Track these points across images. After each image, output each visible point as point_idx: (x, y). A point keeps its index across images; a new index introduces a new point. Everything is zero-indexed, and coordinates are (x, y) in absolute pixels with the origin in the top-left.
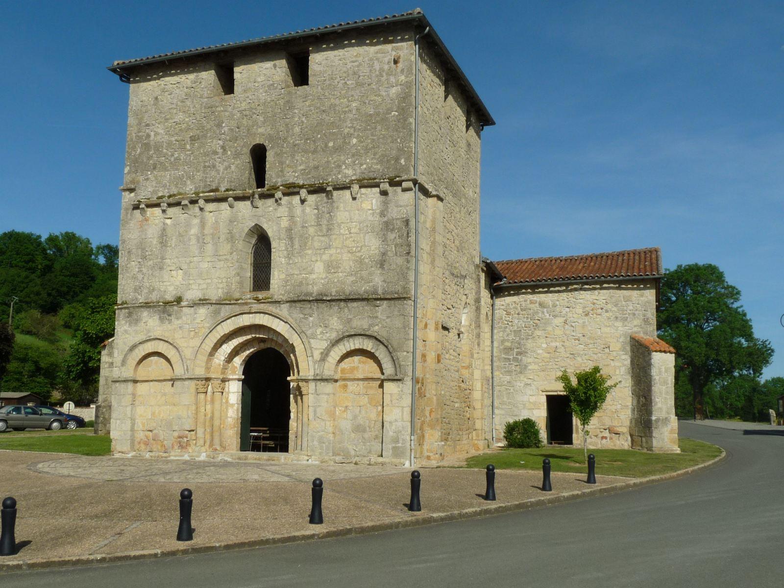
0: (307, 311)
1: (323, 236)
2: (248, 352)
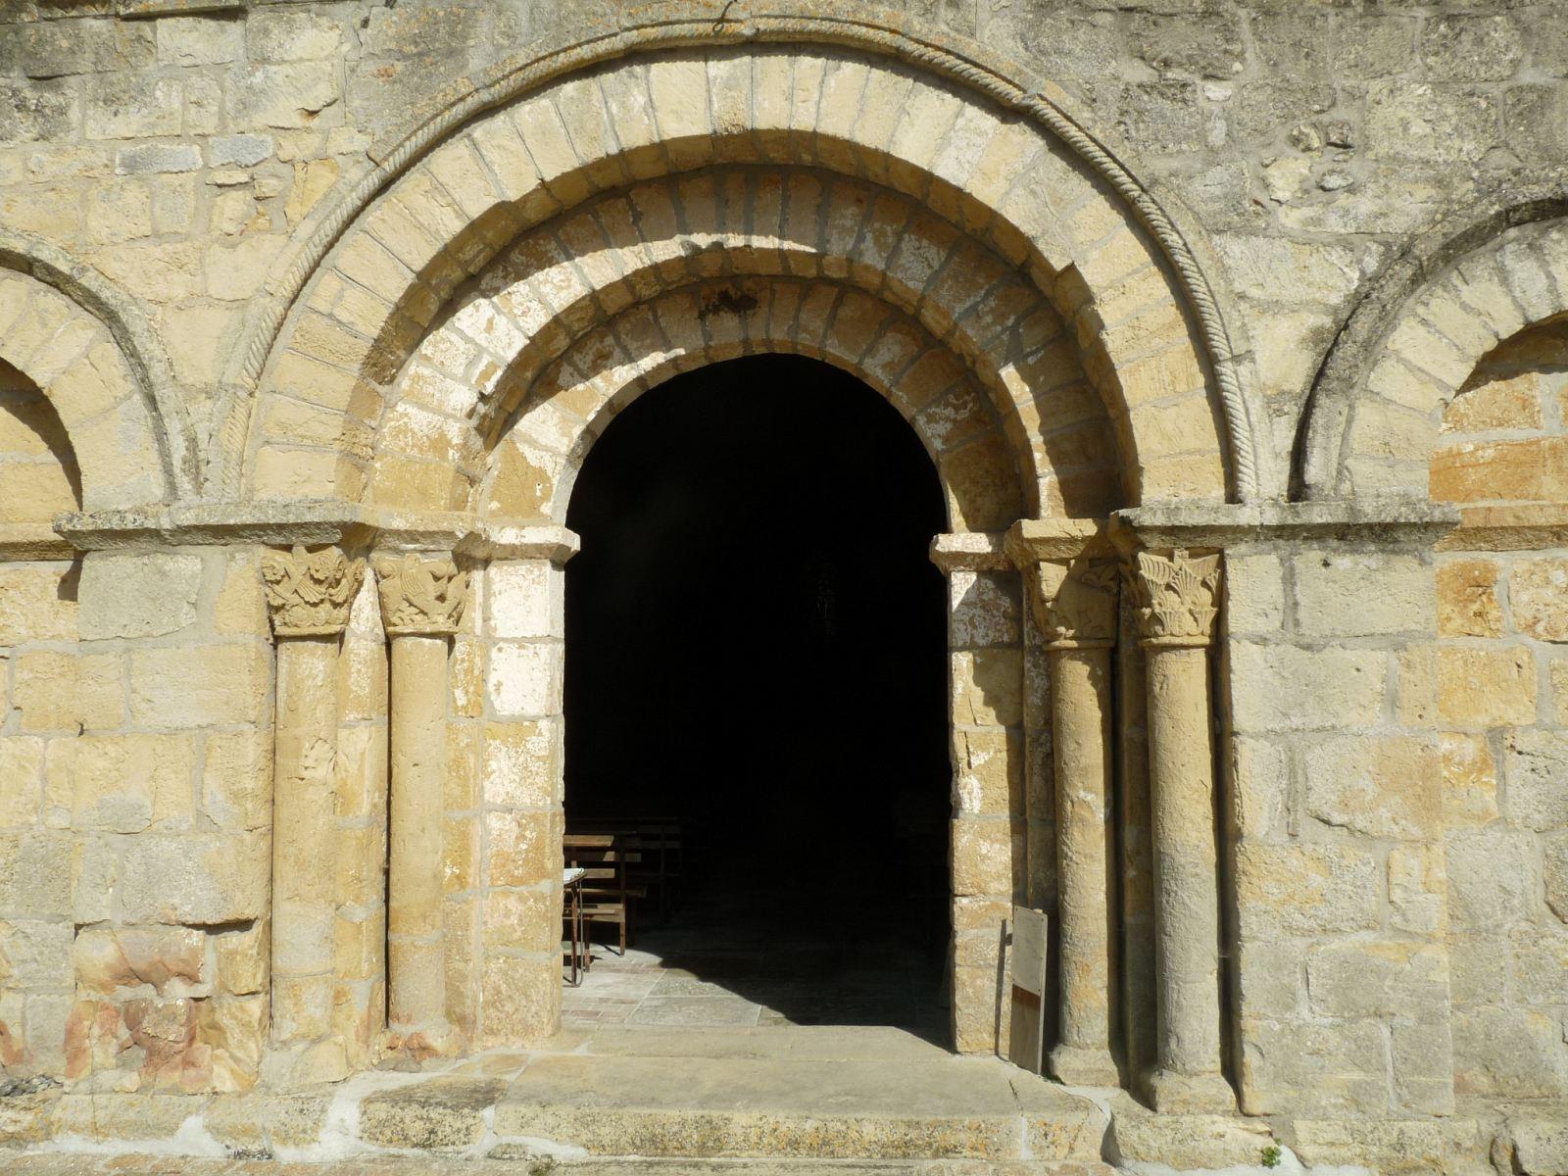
2: (657, 358)
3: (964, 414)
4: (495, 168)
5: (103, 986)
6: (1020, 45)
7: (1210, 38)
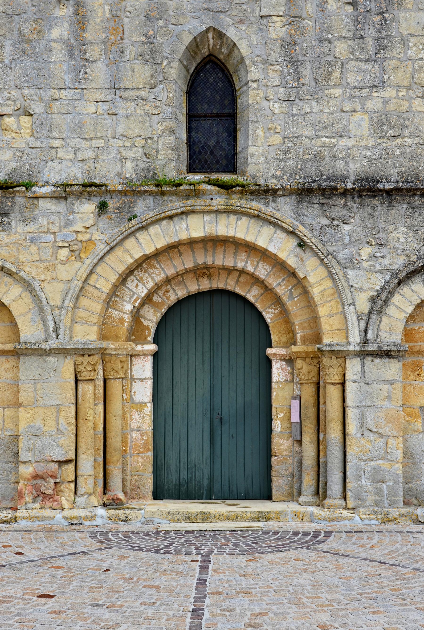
0: (337, 212)
1: (368, 61)
3: (277, 311)
4: (143, 244)
5: (28, 480)
6: (293, 213)
7: (345, 212)
